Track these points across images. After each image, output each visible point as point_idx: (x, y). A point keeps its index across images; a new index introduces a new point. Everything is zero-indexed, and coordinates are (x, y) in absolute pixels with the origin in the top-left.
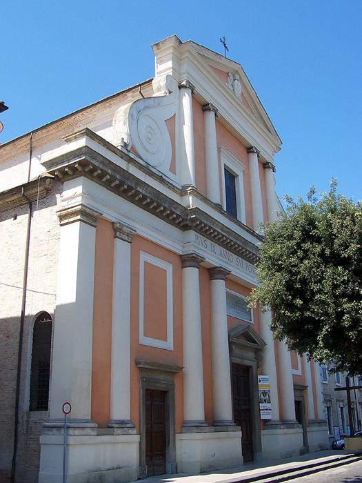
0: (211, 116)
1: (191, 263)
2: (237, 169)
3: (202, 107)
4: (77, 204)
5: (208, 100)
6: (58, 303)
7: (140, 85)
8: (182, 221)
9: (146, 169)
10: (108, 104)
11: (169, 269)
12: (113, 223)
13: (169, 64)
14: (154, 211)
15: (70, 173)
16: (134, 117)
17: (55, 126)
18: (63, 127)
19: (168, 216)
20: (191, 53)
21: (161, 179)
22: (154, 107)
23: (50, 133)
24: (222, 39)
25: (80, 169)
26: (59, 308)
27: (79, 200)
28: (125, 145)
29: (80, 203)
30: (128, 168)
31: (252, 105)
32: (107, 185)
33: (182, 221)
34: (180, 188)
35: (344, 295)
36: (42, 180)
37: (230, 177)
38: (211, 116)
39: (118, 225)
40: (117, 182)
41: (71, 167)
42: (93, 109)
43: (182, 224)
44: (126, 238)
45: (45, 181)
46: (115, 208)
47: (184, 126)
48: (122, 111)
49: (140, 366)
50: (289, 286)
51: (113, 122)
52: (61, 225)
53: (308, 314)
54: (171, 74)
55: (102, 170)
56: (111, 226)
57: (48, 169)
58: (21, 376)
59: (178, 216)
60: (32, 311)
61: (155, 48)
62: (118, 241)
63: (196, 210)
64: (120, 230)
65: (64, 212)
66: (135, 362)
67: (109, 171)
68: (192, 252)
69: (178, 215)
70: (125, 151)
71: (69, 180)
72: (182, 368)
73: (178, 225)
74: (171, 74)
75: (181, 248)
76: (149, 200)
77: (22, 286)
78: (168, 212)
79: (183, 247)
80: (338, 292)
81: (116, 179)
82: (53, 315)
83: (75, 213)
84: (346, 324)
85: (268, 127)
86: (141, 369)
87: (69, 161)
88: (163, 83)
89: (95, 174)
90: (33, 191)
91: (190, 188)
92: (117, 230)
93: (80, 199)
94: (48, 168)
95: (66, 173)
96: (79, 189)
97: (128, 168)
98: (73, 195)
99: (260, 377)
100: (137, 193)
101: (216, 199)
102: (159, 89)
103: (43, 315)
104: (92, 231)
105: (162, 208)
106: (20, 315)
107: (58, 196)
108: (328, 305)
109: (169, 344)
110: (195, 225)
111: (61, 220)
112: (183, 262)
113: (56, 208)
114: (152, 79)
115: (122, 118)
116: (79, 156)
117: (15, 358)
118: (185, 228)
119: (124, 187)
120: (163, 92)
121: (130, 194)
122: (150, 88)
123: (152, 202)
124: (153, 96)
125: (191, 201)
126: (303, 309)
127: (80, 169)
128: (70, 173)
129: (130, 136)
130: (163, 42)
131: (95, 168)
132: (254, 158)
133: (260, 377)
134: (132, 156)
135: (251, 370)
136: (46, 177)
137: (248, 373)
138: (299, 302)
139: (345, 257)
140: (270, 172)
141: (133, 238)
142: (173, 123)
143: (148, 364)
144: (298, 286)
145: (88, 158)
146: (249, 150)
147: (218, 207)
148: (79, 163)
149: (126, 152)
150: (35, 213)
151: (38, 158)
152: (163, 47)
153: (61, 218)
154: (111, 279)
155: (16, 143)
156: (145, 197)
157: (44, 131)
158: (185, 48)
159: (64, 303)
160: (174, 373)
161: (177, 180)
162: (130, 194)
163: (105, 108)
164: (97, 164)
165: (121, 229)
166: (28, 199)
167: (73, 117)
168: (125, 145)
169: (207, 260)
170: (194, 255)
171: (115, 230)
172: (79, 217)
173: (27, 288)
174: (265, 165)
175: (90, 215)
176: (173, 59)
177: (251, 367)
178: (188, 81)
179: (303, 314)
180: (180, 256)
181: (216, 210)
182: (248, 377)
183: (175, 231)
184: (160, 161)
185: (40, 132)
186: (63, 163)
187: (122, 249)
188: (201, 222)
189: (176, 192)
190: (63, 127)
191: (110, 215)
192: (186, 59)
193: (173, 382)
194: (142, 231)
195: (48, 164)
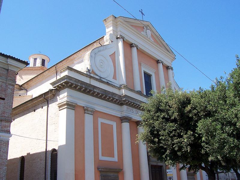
0: (134, 50)
1: (125, 121)
2: (149, 72)
3: (129, 46)
4: (65, 101)
5: (133, 42)
6: (59, 145)
7: (99, 39)
8: (120, 101)
9: (100, 80)
10: (86, 49)
11: (114, 124)
12: (83, 107)
13: (111, 28)
14: (104, 99)
15: (62, 87)
16: (92, 57)
17: (65, 61)
18: (69, 61)
19: (112, 100)
20: (121, 22)
21: (108, 83)
22: (103, 50)
23: (64, 64)
24: (141, 10)
25: (65, 85)
26: (59, 147)
27: (65, 99)
28: (89, 70)
29: (66, 100)
30: (90, 81)
31: (159, 41)
32: (80, 90)
33: (120, 101)
34: (119, 86)
35: (174, 136)
36: (51, 91)
37: (148, 77)
38: (134, 50)
39: (86, 108)
40: (84, 89)
41: (61, 84)
42: (80, 52)
43: (120, 103)
44: (90, 113)
45: (52, 91)
46: (83, 100)
47: (120, 57)
48: (87, 55)
49: (99, 170)
50: (152, 132)
51: (84, 60)
52: (59, 110)
53: (161, 145)
54: (112, 33)
55: (75, 84)
56: (83, 108)
57: (53, 86)
58: (46, 177)
59: (117, 100)
60: (50, 149)
61: (104, 21)
62: (86, 115)
63: (126, 96)
64: (87, 110)
65: (60, 105)
66: (97, 168)
67: (79, 84)
68: (125, 115)
69: (117, 99)
70: (88, 74)
71: (62, 90)
72: (122, 170)
73: (118, 104)
74: (112, 33)
75: (120, 114)
76: (100, 95)
77: (45, 139)
78: (112, 98)
79: (121, 113)
80: (171, 135)
81: (83, 87)
82: (57, 150)
83: (64, 105)
84: (176, 149)
85: (167, 49)
86: (100, 171)
87: (60, 82)
88: (108, 38)
89: (73, 86)
90: (48, 96)
91: (123, 86)
92: (85, 110)
93: (66, 98)
94: (53, 85)
95: (60, 87)
96: (66, 94)
97: (90, 81)
98: (63, 97)
99: (167, 170)
100: (95, 92)
101: (138, 88)
102: (107, 41)
103: (54, 150)
104: (73, 112)
105: (108, 97)
106: (45, 150)
107: (58, 97)
108: (169, 141)
109: (116, 159)
110: (126, 103)
111: (59, 108)
112: (121, 120)
113: (57, 103)
114: (103, 37)
115: (87, 58)
116: (64, 80)
117: (44, 169)
118: (122, 104)
119: (87, 90)
120: (109, 42)
121: (91, 93)
122: (103, 40)
123: (102, 95)
124: (105, 44)
125: (123, 92)
126: (159, 142)
127: (65, 85)
128: (62, 87)
129: (91, 66)
130: (107, 18)
131: (72, 84)
132: (161, 65)
133: (167, 170)
134: (92, 75)
135: (162, 167)
136: (52, 90)
137: (161, 169)
138: (156, 140)
139: (172, 119)
140: (170, 71)
141: (94, 113)
142: (114, 56)
143: (103, 169)
144: (156, 132)
145: (68, 80)
146: (158, 62)
147: (140, 93)
148: (64, 82)
149: (89, 74)
150: (50, 105)
151: (59, 76)
152: (108, 21)
153: (60, 107)
154: (84, 132)
155: (50, 70)
156: (98, 94)
157: (61, 63)
158: (118, 20)
159: (61, 145)
160: (118, 172)
161: (117, 83)
162: (91, 93)
163: (85, 51)
164: (73, 82)
165: (87, 109)
166: (46, 99)
167: (72, 56)
168: (89, 70)
169: (133, 118)
170: (126, 117)
171: (85, 110)
172: (66, 107)
173: (48, 140)
174: (167, 68)
175: (71, 105)
176: (113, 26)
177: (162, 166)
178: (121, 35)
179: (159, 145)
180: (120, 117)
181: (138, 94)
182: (161, 171)
183: (116, 107)
184: (107, 75)
185: (59, 64)
186: (58, 83)
187: (89, 119)
188: (129, 101)
189: (116, 88)
190: (69, 61)
191: (81, 103)
192: (119, 25)
193: (118, 176)
194: (98, 108)
195: (53, 84)
